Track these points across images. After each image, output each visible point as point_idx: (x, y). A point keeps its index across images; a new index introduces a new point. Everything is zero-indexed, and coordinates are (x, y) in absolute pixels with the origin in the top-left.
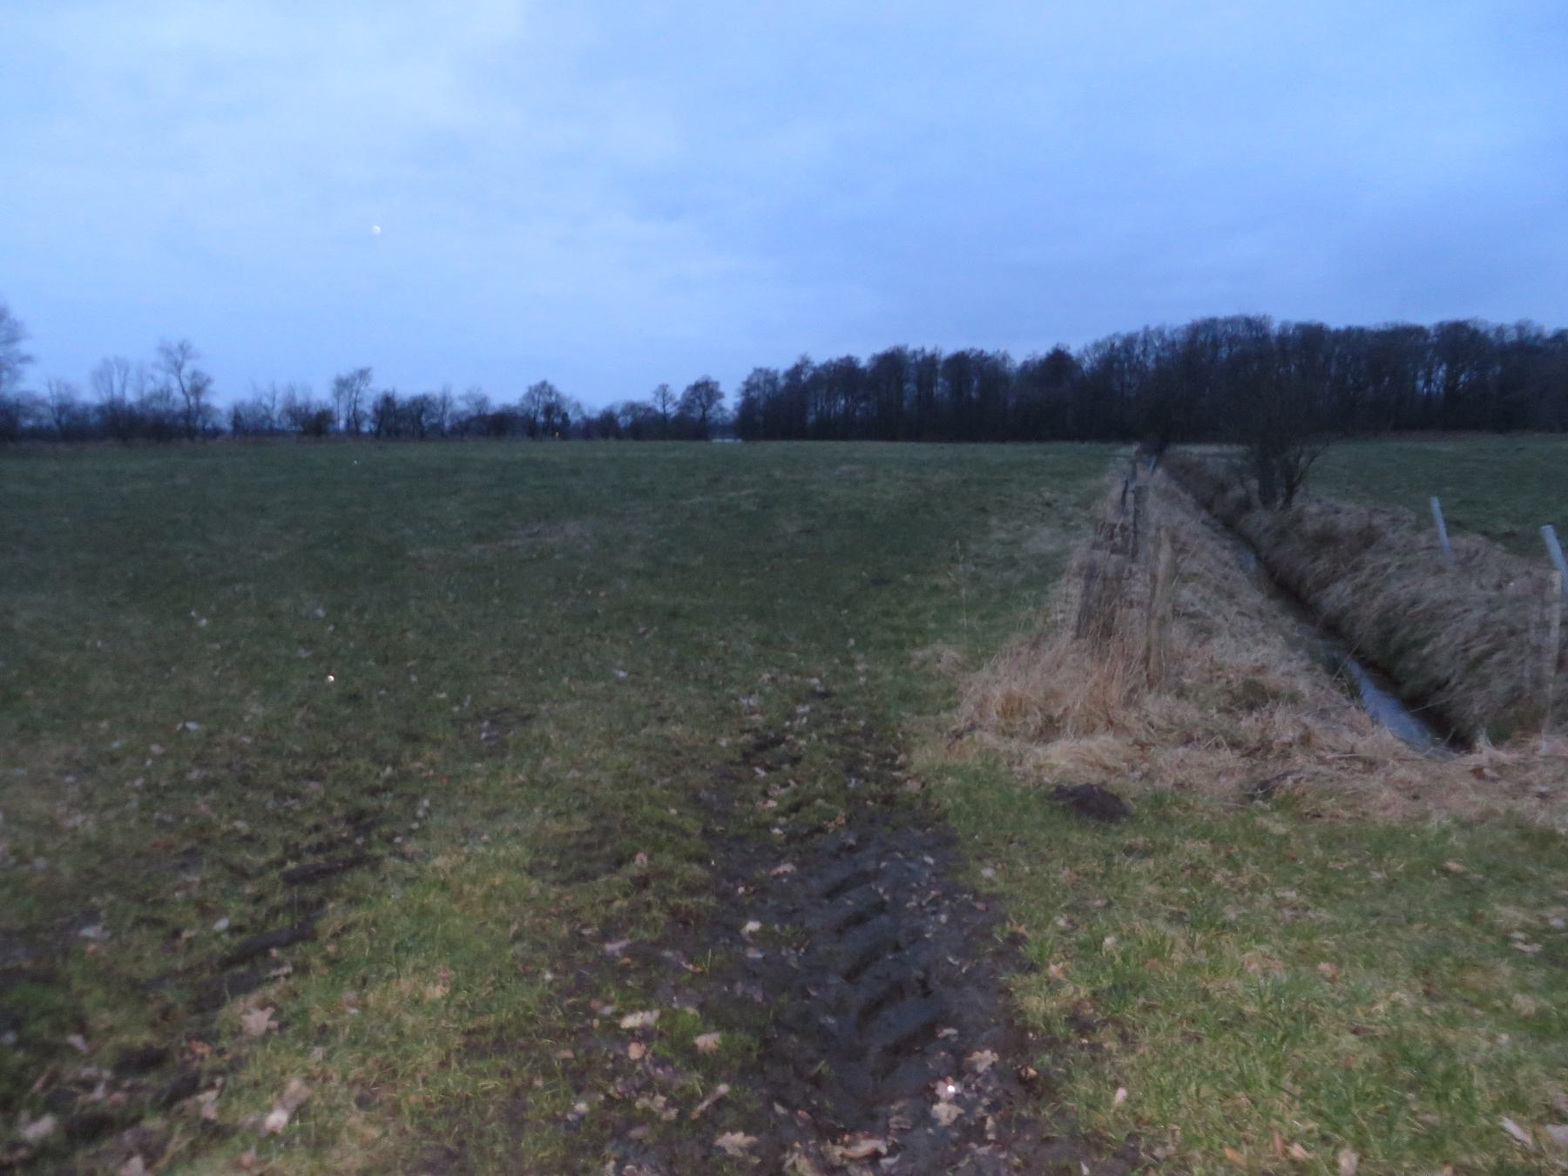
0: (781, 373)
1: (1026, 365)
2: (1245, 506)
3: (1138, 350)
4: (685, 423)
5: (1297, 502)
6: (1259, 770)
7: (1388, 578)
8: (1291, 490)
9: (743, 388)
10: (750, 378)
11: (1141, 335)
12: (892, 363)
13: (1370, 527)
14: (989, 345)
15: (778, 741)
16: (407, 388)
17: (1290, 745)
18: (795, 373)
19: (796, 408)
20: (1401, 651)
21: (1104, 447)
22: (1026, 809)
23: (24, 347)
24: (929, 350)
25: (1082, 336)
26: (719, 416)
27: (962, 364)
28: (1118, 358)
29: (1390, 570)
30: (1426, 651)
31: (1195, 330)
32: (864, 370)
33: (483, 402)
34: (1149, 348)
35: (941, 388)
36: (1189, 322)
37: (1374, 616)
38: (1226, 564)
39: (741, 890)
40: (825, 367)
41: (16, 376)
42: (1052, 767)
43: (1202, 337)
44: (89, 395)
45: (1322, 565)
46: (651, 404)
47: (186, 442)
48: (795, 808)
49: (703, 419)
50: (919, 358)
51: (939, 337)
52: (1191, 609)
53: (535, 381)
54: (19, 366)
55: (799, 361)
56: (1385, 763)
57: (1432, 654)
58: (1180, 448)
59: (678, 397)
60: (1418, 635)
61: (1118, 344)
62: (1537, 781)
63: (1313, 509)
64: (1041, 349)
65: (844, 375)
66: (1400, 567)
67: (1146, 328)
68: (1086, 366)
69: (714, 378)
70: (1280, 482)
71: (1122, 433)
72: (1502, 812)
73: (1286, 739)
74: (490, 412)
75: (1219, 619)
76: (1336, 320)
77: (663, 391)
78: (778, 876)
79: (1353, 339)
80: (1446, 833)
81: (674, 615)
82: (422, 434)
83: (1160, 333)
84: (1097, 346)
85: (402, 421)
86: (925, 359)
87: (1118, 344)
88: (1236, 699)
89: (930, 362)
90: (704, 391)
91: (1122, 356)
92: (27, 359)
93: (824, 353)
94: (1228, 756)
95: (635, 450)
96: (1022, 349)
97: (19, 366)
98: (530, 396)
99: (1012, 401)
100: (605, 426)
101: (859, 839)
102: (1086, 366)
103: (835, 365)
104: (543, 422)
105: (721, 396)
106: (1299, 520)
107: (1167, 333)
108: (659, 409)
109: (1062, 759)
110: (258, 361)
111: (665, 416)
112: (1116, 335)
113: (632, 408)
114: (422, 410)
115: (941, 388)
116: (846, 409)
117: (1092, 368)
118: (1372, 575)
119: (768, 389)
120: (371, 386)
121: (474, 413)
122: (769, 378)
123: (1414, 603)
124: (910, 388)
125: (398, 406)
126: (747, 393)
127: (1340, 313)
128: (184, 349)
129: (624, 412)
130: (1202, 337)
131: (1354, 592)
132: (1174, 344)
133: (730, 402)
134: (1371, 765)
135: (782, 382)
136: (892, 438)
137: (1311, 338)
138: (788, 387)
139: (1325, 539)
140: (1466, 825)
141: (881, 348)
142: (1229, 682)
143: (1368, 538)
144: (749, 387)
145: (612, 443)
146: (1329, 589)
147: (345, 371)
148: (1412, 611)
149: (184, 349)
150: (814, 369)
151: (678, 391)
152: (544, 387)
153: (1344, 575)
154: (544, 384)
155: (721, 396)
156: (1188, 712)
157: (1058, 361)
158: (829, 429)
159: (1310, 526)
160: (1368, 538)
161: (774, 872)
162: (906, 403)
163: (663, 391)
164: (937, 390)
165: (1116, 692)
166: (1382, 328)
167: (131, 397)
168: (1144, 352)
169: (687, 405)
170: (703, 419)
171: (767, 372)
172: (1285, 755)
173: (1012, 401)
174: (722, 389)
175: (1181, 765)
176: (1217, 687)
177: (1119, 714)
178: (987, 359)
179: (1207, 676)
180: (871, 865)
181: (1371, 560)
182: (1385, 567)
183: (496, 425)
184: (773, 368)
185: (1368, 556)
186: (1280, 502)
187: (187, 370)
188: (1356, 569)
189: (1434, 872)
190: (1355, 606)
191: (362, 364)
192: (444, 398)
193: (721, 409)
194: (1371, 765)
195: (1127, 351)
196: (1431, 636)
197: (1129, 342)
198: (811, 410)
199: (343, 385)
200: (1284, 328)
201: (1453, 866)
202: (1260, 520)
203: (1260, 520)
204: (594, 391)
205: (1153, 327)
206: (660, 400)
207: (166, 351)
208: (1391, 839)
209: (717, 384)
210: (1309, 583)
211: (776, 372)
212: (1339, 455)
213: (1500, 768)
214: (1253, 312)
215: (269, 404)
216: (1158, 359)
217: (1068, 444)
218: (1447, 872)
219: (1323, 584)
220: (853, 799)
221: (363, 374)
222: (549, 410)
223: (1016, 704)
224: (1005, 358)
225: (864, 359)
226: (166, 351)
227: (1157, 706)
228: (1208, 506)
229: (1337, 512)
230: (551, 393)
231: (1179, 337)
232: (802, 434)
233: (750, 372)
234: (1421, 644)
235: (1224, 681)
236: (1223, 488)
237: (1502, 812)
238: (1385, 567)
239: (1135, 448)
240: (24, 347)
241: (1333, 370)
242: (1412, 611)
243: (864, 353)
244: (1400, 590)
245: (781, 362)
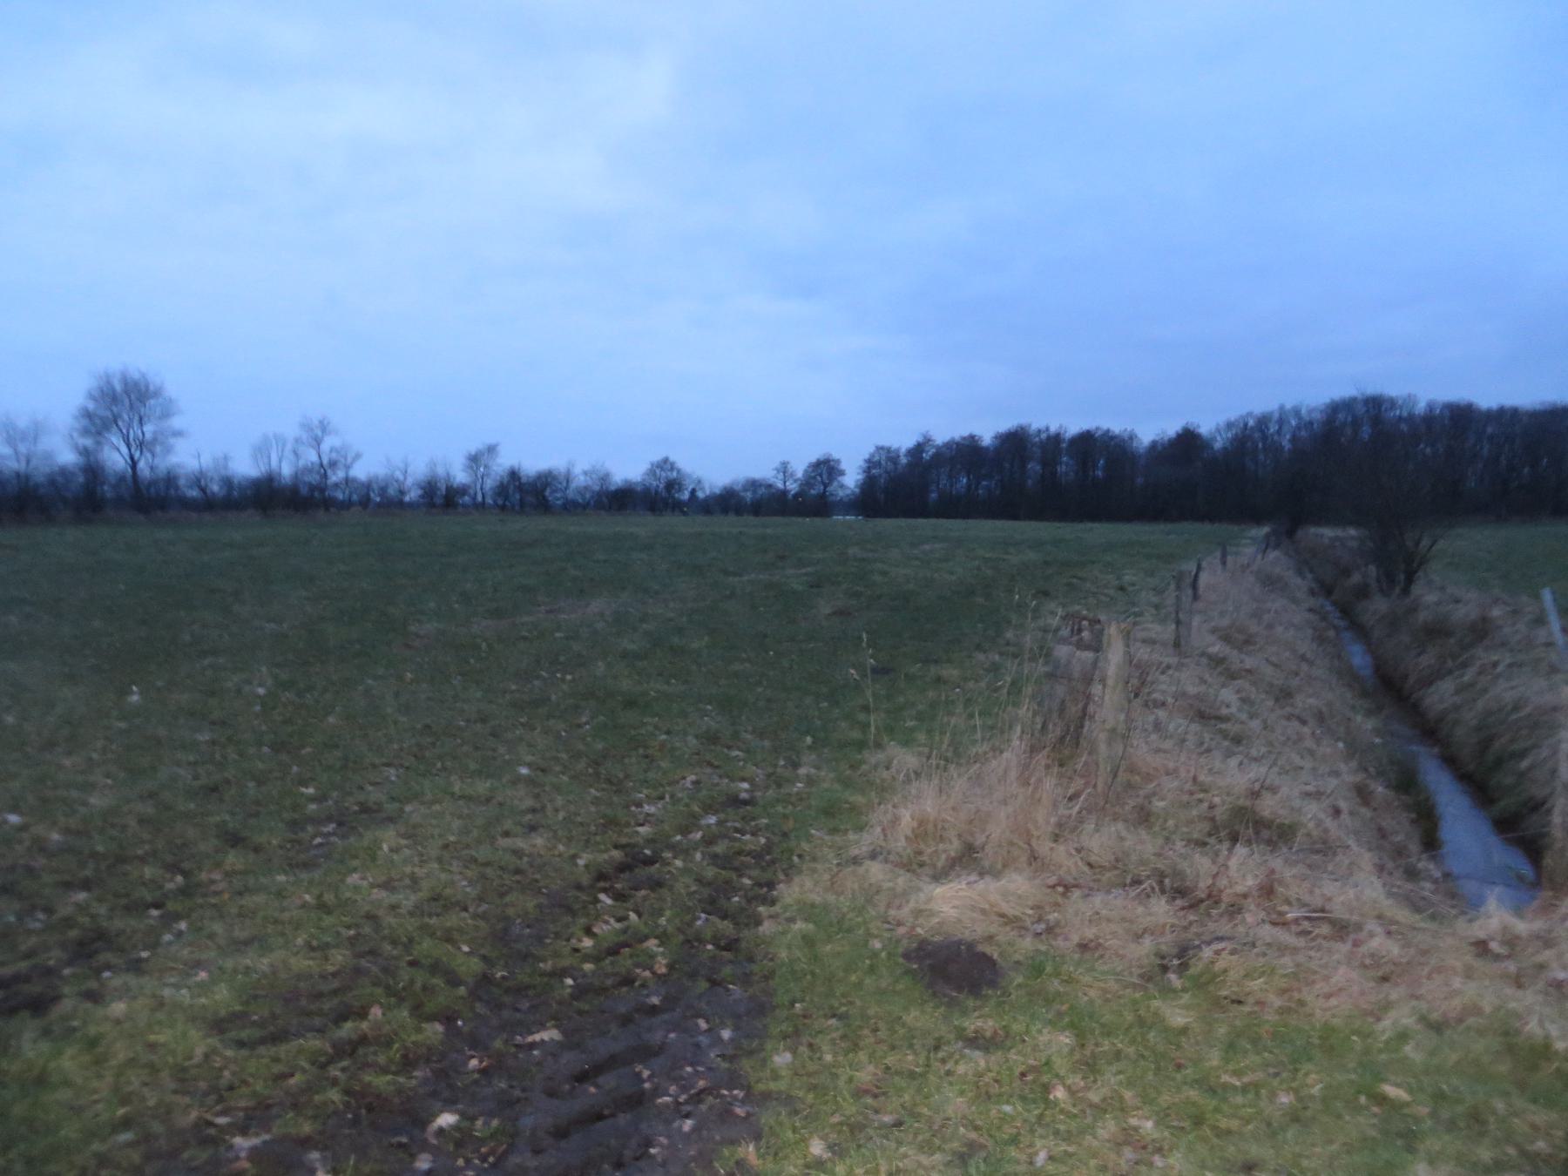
0: (903, 450)
1: (1154, 444)
2: (1363, 592)
3: (1273, 428)
4: (808, 500)
5: (1417, 589)
6: (1194, 929)
7: (1498, 676)
8: (1410, 580)
9: (865, 465)
10: (872, 455)
11: (1276, 416)
12: (1015, 442)
13: (1484, 619)
14: (1116, 425)
15: (649, 862)
16: (532, 463)
17: (1245, 896)
18: (918, 449)
19: (913, 486)
20: (1499, 762)
21: (1236, 528)
22: (872, 970)
23: (176, 422)
24: (1053, 429)
25: (1212, 418)
26: (841, 493)
27: (1087, 444)
28: (1251, 439)
29: (1500, 669)
30: (1524, 764)
31: (1335, 408)
32: (987, 449)
33: (605, 478)
34: (1285, 428)
35: (1066, 467)
36: (1328, 401)
37: (1474, 722)
38: (1303, 658)
39: (474, 1063)
40: (948, 445)
41: (168, 450)
42: (932, 914)
43: (1341, 416)
44: (245, 467)
45: (1427, 660)
46: (772, 481)
47: (321, 513)
48: (614, 951)
49: (823, 496)
50: (1044, 436)
51: (1067, 418)
52: (1224, 711)
53: (657, 457)
54: (172, 441)
55: (921, 440)
56: (1359, 927)
57: (1531, 768)
58: (1313, 530)
59: (800, 474)
60: (1516, 747)
61: (1251, 423)
62: (1554, 965)
63: (1431, 598)
64: (1171, 428)
65: (966, 453)
66: (1510, 666)
67: (1282, 408)
68: (1218, 445)
69: (835, 456)
70: (1401, 569)
71: (1255, 516)
72: (1488, 1009)
73: (1240, 889)
74: (613, 488)
75: (1255, 724)
76: (1488, 397)
77: (784, 469)
78: (533, 1045)
79: (1506, 418)
80: (1403, 1036)
81: (630, 703)
82: (677, 507)
83: (1297, 412)
84: (1229, 425)
85: (529, 496)
86: (1049, 438)
87: (1251, 423)
88: (1214, 831)
89: (1056, 439)
90: (826, 469)
91: (1257, 435)
92: (178, 434)
93: (945, 431)
94: (1161, 910)
95: (775, 526)
96: (1150, 427)
97: (172, 441)
98: (652, 472)
99: (1140, 480)
100: (728, 502)
101: (665, 999)
102: (1218, 445)
103: (958, 444)
104: (660, 497)
105: (842, 473)
106: (1413, 610)
107: (1303, 411)
108: (780, 485)
109: (950, 905)
110: (397, 441)
111: (784, 493)
112: (1250, 414)
113: (753, 484)
114: (547, 484)
115: (1066, 467)
116: (969, 486)
117: (1225, 449)
118: (1480, 673)
119: (890, 466)
120: (499, 460)
121: (597, 488)
122: (891, 455)
123: (1516, 708)
124: (1034, 467)
125: (524, 480)
126: (867, 471)
127: (1492, 390)
128: (324, 427)
129: (745, 489)
130: (1341, 416)
131: (1457, 692)
132: (1311, 423)
133: (851, 479)
134: (1342, 929)
135: (904, 460)
136: (1015, 518)
137: (1461, 418)
138: (909, 464)
139: (1436, 631)
140: (1437, 1027)
141: (1006, 425)
142: (1212, 807)
143: (1481, 631)
144: (871, 464)
145: (732, 518)
146: (1433, 689)
147: (473, 448)
148: (1514, 717)
149: (324, 427)
150: (938, 448)
151: (799, 468)
152: (665, 464)
153: (1450, 672)
154: (666, 460)
155: (842, 473)
156: (1143, 846)
157: (1188, 440)
158: (953, 508)
159: (1422, 616)
160: (1481, 631)
161: (530, 1039)
162: (1030, 482)
163: (784, 469)
164: (1062, 469)
165: (1044, 820)
166: (1538, 407)
167: (287, 471)
168: (1279, 432)
169: (807, 482)
170: (823, 496)
171: (889, 450)
172: (1235, 910)
173: (1140, 480)
174: (843, 466)
175: (1096, 918)
176: (1195, 812)
177: (1044, 847)
178: (1113, 438)
179: (1185, 798)
180: (657, 1037)
181: (1483, 656)
182: (1495, 665)
183: (619, 499)
184: (895, 446)
185: (1479, 651)
186: (1397, 590)
187: (325, 446)
188: (1465, 665)
189: (1363, 1099)
190: (1457, 708)
191: (491, 440)
192: (568, 473)
193: (842, 486)
194: (1342, 929)
195: (1262, 431)
196: (1535, 746)
197: (1263, 421)
198: (933, 487)
199: (474, 459)
200: (1431, 407)
201: (1391, 1091)
202: (1378, 606)
203: (1378, 606)
204: (714, 468)
205: (1288, 406)
206: (781, 476)
207: (306, 426)
208: (1330, 1044)
209: (838, 461)
210: (1411, 681)
211: (898, 450)
212: (1472, 540)
213: (1512, 941)
214: (1372, 389)
215: (401, 478)
216: (1294, 439)
217: (1197, 525)
218: (1382, 1100)
219: (1428, 681)
220: (693, 942)
221: (492, 450)
222: (672, 485)
223: (930, 827)
224: (1132, 437)
225: (987, 437)
226: (306, 426)
227: (1100, 840)
228: (1327, 590)
229: (1457, 601)
230: (672, 469)
231: (1317, 416)
232: (924, 512)
233: (872, 450)
234: (1522, 754)
235: (1206, 805)
236: (1346, 572)
237: (1488, 1009)
238: (1495, 665)
239: (1266, 530)
240: (176, 422)
241: (1485, 451)
242: (1514, 717)
243: (987, 431)
244: (1504, 692)
245: (903, 441)
